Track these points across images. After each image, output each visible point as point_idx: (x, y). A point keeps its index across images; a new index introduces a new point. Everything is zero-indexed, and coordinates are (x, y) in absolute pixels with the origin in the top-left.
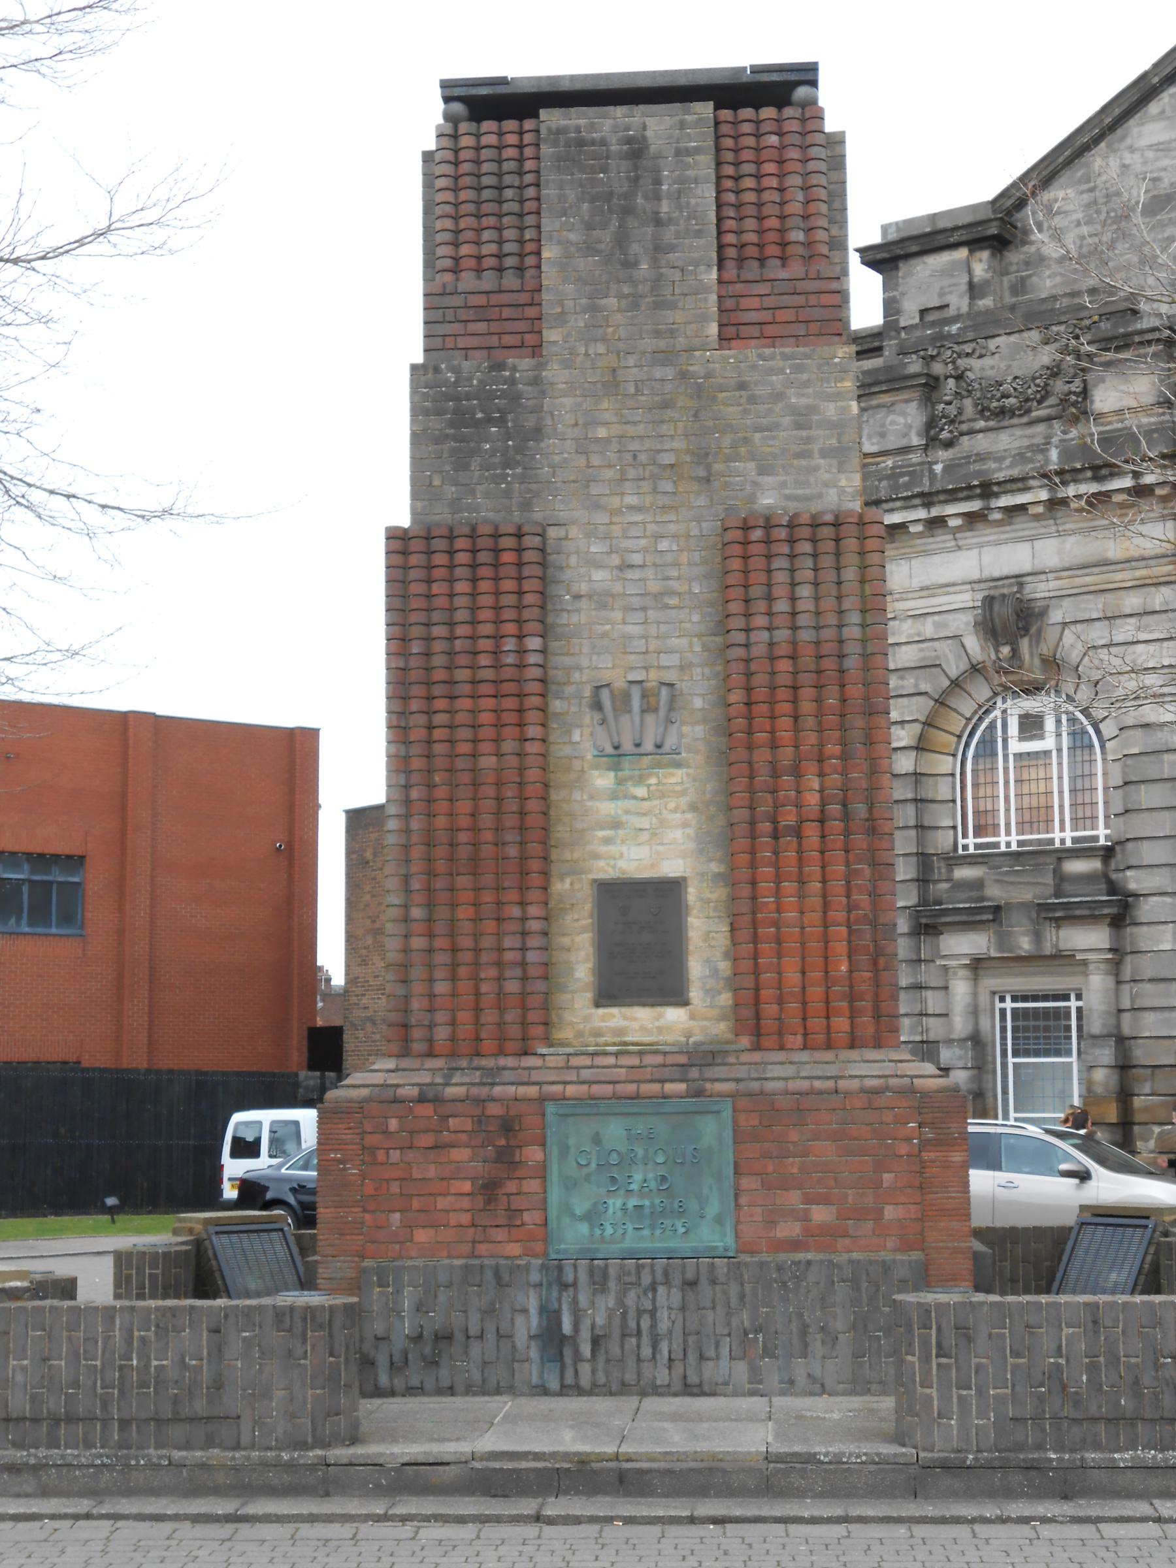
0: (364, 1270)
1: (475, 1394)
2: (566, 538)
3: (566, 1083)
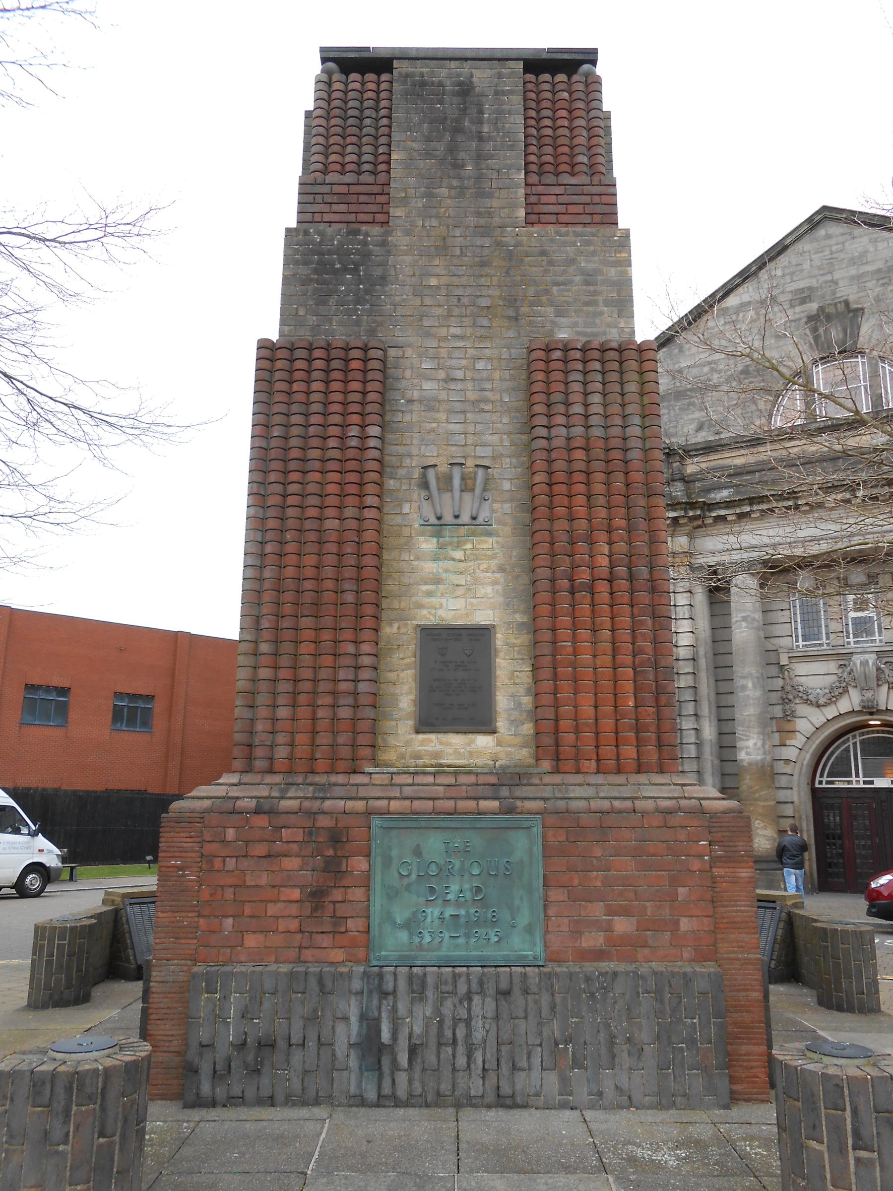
0: (194, 976)
1: (294, 1104)
2: (403, 357)
3: (390, 799)
